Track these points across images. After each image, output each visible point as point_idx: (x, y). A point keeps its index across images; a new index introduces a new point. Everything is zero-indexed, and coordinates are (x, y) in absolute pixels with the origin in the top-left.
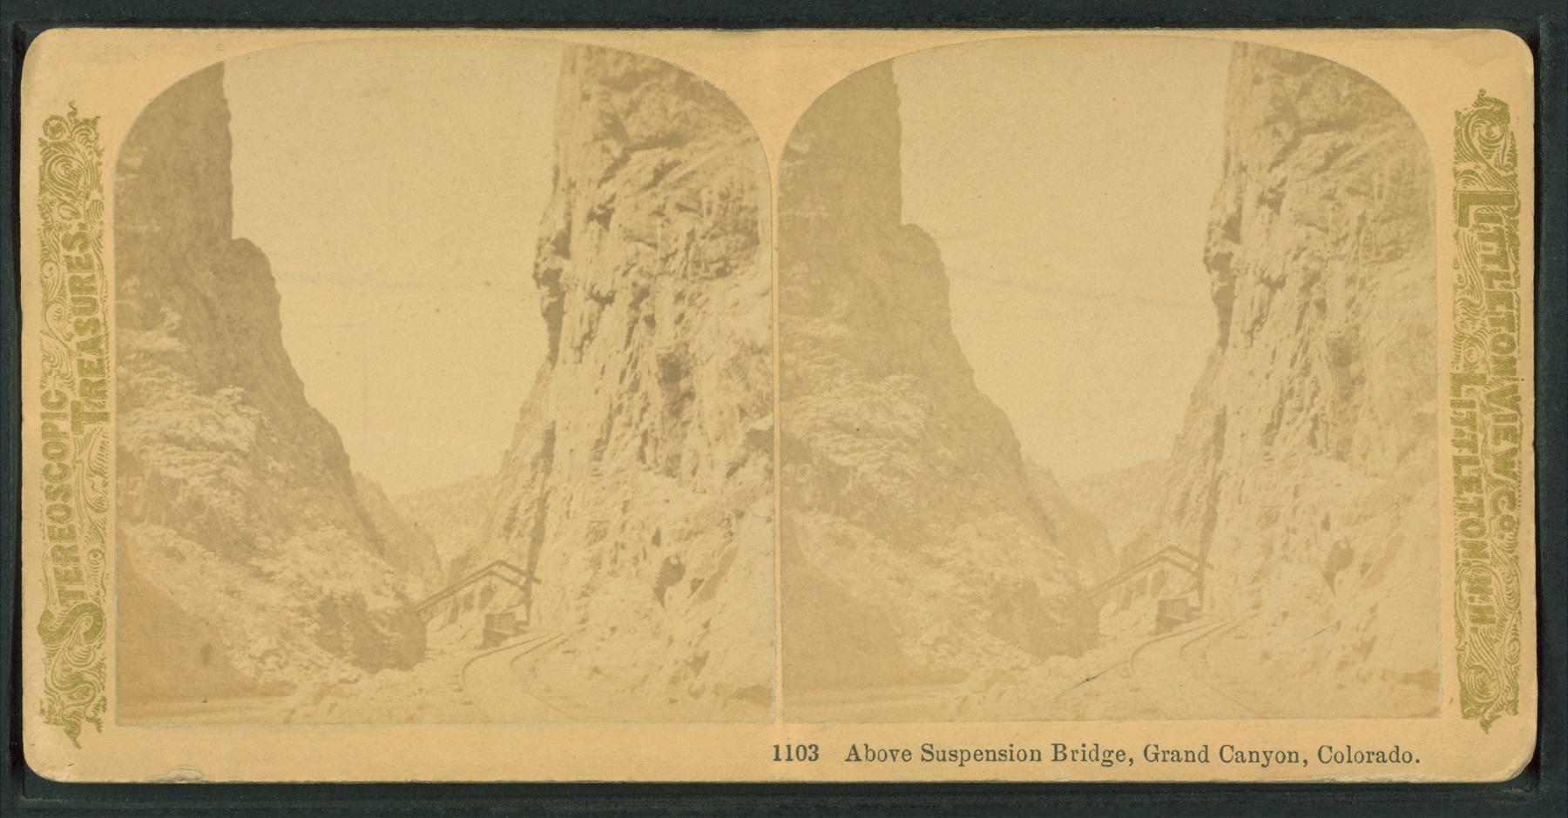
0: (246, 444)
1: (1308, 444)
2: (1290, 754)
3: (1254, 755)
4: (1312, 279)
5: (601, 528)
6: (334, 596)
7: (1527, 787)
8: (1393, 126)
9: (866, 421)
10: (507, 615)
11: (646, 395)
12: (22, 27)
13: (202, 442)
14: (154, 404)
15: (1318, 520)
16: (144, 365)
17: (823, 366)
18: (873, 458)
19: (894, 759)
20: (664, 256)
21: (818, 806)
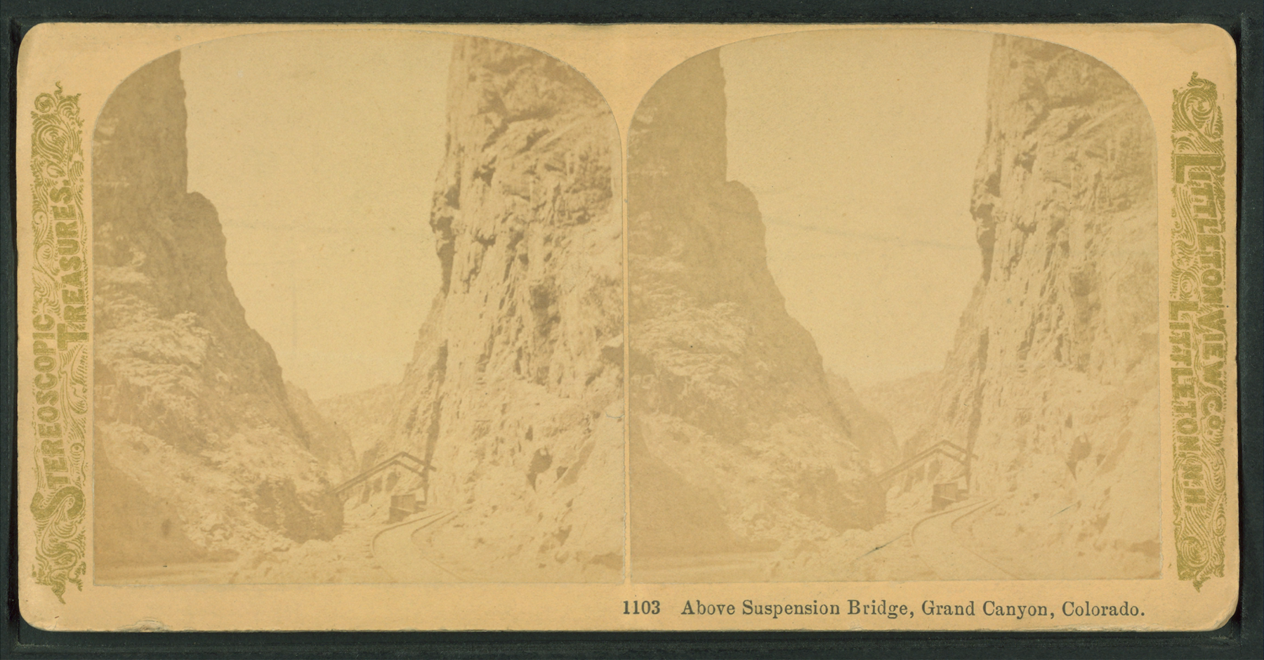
0: (198, 358)
1: (1055, 359)
2: (1040, 608)
3: (1011, 609)
4: (1058, 225)
5: (485, 426)
6: (269, 481)
7: (1231, 635)
8: (1123, 102)
9: (159, 350)
10: (408, 496)
11: (521, 319)
12: (18, 22)
13: (163, 357)
14: (124, 326)
15: (1062, 420)
16: (116, 295)
17: (664, 295)
18: (704, 369)
19: (721, 612)
20: (535, 206)
21: (659, 650)
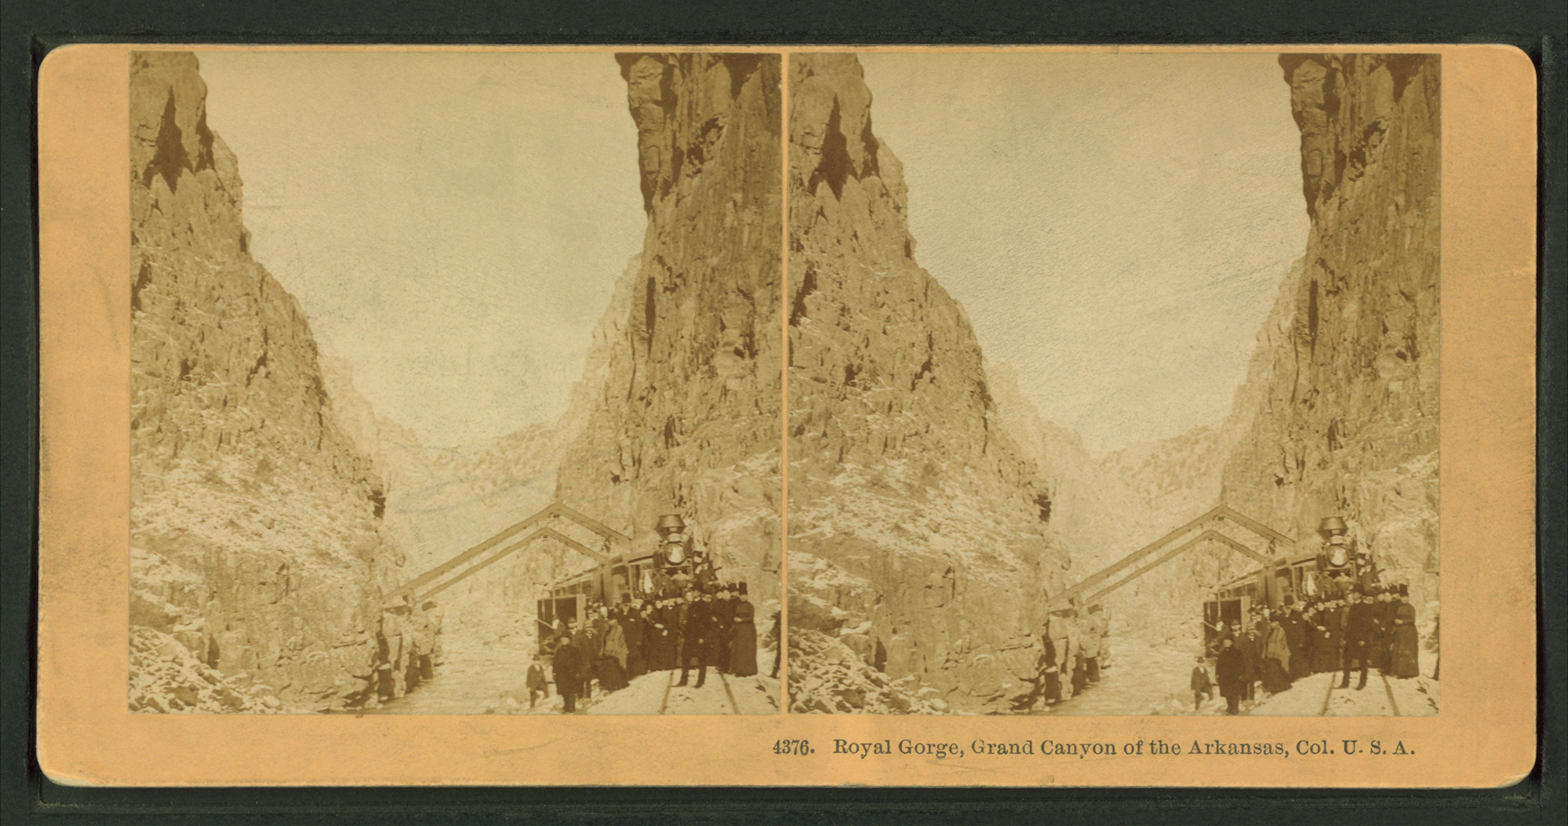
2: (1107, 746)
3: (1072, 748)
7: (1529, 794)
12: (40, 39)
21: (827, 812)
